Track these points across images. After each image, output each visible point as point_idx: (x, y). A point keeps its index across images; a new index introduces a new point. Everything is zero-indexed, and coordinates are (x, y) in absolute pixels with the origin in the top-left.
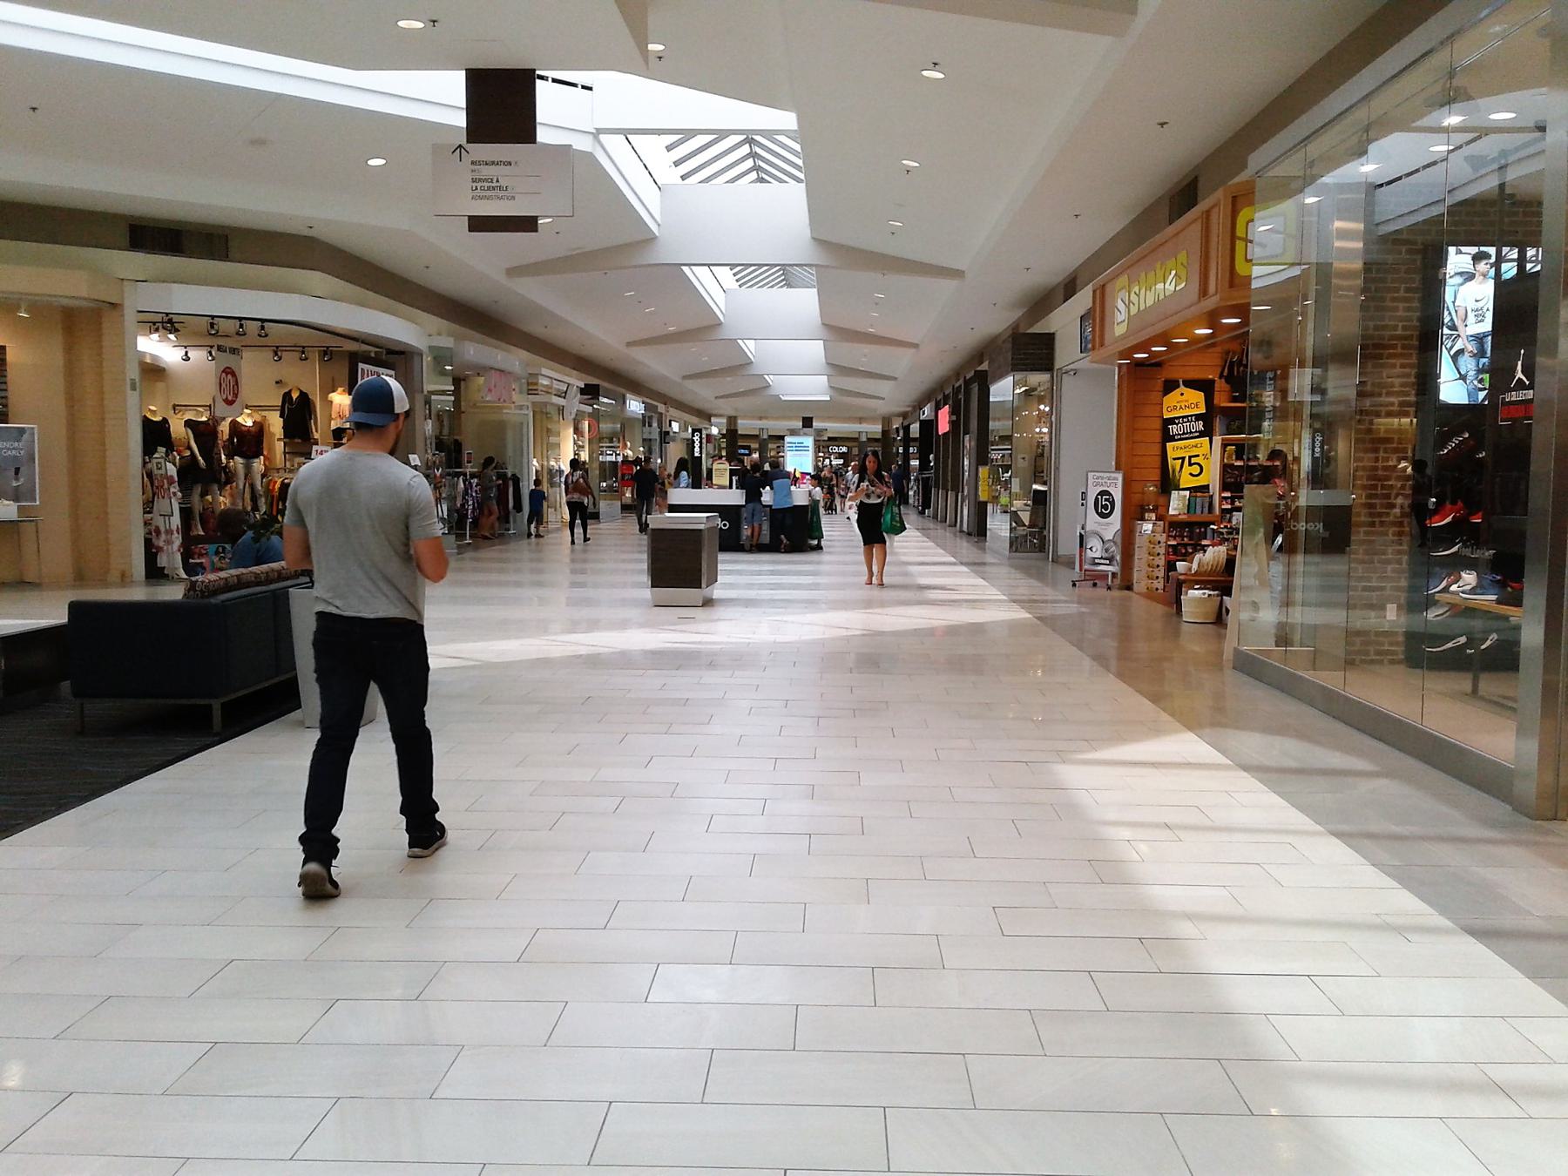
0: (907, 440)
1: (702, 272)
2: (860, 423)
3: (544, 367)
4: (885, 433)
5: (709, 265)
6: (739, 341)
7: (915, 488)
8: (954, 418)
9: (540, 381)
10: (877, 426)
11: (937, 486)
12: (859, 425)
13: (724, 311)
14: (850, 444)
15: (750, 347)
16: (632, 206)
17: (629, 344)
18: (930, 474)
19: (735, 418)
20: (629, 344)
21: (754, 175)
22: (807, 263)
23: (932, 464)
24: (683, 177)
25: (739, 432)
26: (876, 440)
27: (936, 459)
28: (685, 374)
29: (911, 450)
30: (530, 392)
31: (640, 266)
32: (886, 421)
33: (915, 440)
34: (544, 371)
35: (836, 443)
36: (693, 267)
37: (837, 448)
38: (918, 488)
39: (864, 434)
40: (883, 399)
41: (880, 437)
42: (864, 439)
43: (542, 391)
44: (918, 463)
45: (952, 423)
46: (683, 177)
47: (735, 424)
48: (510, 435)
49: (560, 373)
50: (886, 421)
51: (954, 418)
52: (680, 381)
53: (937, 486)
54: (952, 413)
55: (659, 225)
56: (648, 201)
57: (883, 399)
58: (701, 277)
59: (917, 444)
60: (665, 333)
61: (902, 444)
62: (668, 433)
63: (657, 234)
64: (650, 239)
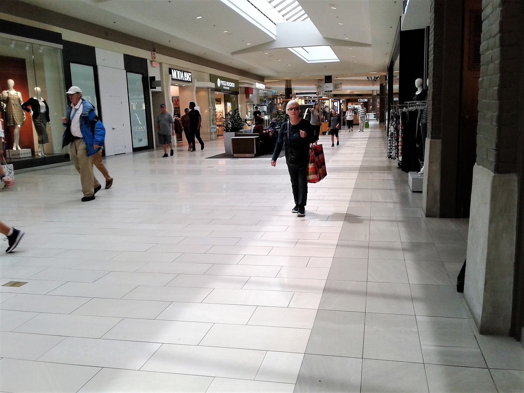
2: (373, 86)
12: (373, 87)
14: (369, 97)
19: (290, 81)
37: (362, 100)
38: (396, 129)
44: (398, 99)
47: (290, 85)
64: (273, 41)
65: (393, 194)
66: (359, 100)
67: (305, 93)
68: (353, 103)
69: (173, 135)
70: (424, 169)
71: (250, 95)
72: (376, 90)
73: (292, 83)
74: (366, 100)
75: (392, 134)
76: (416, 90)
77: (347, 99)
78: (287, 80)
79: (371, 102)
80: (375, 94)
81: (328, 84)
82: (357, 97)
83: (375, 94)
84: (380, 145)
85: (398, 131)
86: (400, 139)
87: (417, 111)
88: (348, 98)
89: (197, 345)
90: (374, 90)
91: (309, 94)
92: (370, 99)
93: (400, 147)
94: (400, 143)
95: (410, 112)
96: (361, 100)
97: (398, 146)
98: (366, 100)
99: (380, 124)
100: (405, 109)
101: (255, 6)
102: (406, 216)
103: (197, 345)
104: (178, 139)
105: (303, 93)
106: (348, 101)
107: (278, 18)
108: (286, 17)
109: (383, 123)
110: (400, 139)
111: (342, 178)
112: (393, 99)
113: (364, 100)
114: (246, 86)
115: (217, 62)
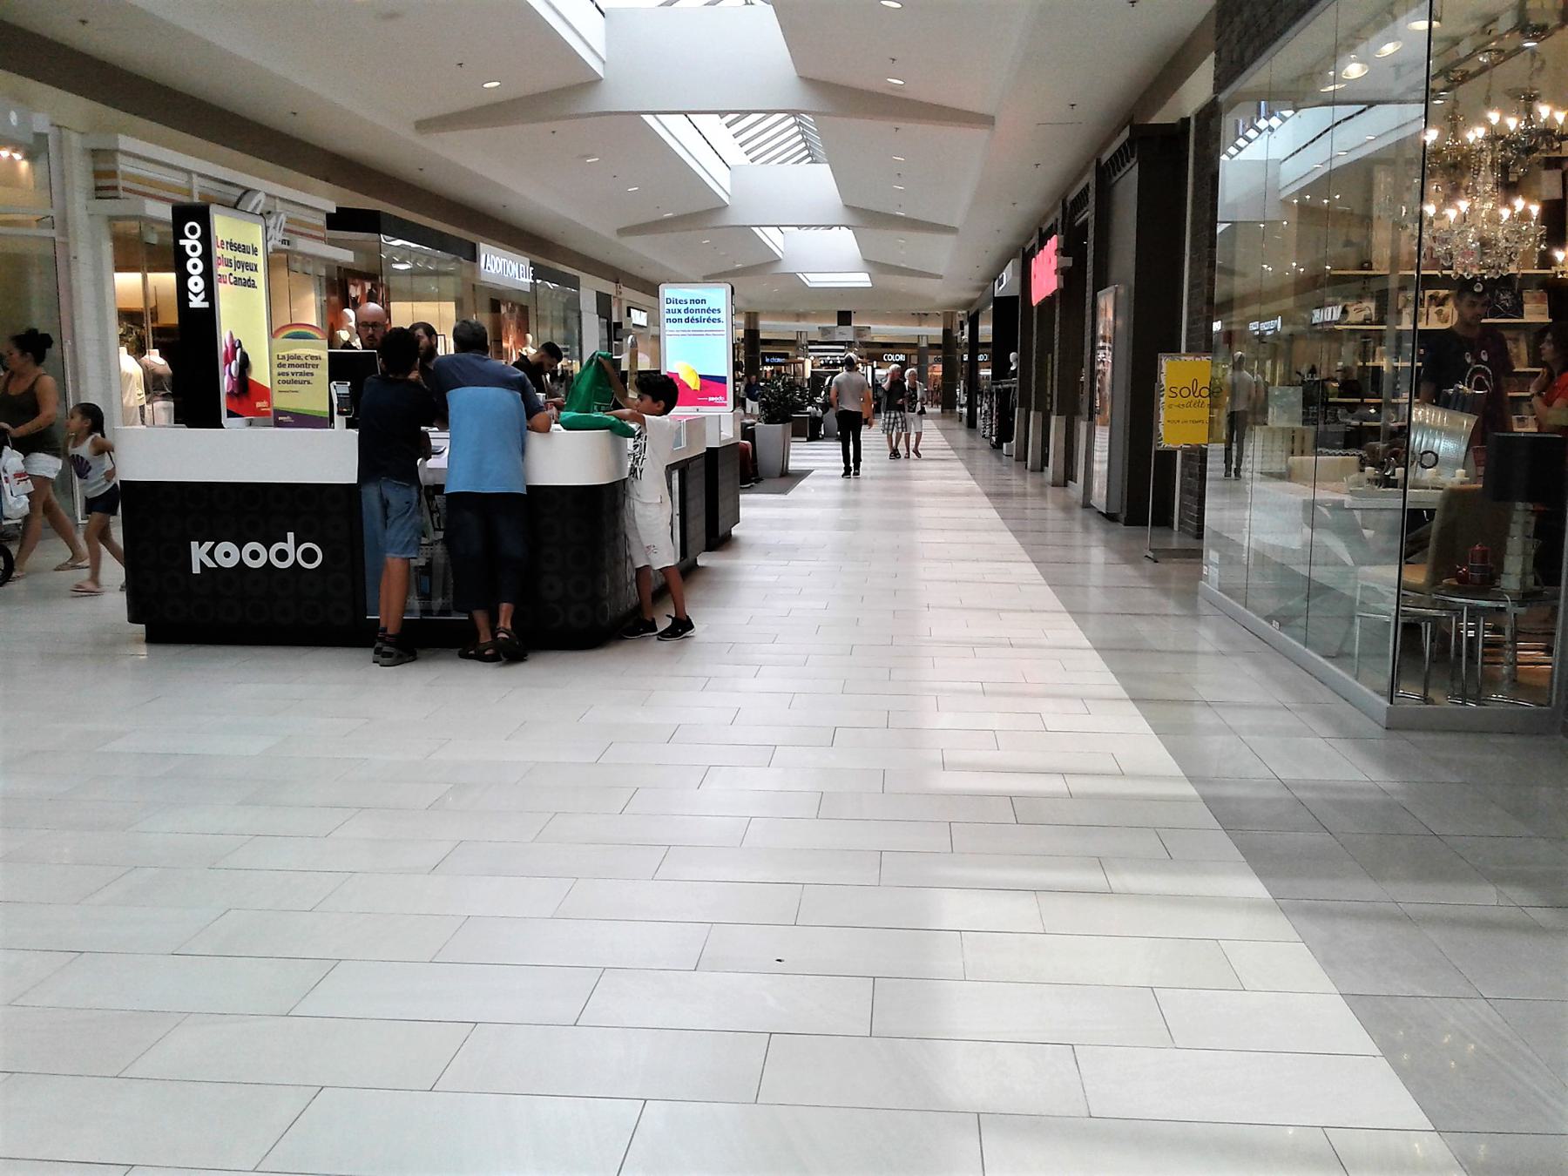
0: (974, 345)
1: (676, 123)
2: (920, 325)
3: (121, 132)
4: (947, 333)
5: (778, 226)
6: (755, 229)
7: (986, 406)
8: (1069, 262)
9: (121, 167)
10: (936, 329)
11: (1025, 403)
12: (918, 328)
13: (729, 192)
14: (909, 351)
15: (773, 238)
16: (583, 60)
17: (423, 126)
18: (1013, 383)
19: (756, 314)
20: (423, 126)
21: (809, 159)
22: (806, 109)
23: (1013, 368)
24: (752, 161)
25: (762, 336)
26: (938, 346)
27: (1024, 361)
28: (424, 115)
29: (981, 358)
30: (101, 194)
31: (719, 227)
32: (948, 317)
33: (986, 345)
34: (126, 143)
35: (891, 350)
36: (658, 116)
37: (892, 357)
38: (991, 407)
39: (924, 338)
40: (940, 277)
41: (941, 342)
42: (924, 344)
43: (125, 189)
44: (990, 373)
45: (1063, 272)
46: (752, 161)
47: (756, 323)
48: (36, 283)
49: (205, 158)
50: (948, 317)
51: (1069, 262)
52: (615, 238)
53: (1025, 403)
54: (1063, 251)
55: (604, 62)
56: (719, 179)
57: (940, 277)
58: (675, 131)
59: (990, 350)
60: (658, 218)
61: (967, 350)
62: (619, 325)
63: (602, 76)
64: (721, 208)
66: (886, 357)
70: (1014, 442)
72: (927, 336)
73: (760, 317)
75: (986, 412)
76: (1011, 365)
78: (749, 313)
83: (924, 344)
84: (885, 490)
85: (992, 409)
86: (994, 418)
87: (1010, 388)
89: (431, 1090)
93: (994, 426)
94: (994, 422)
95: (1004, 389)
97: (991, 425)
99: (942, 412)
100: (1000, 386)
102: (993, 489)
103: (431, 1090)
107: (735, 155)
108: (747, 147)
109: (948, 410)
110: (994, 418)
111: (232, 1081)
112: (977, 373)
113: (898, 358)
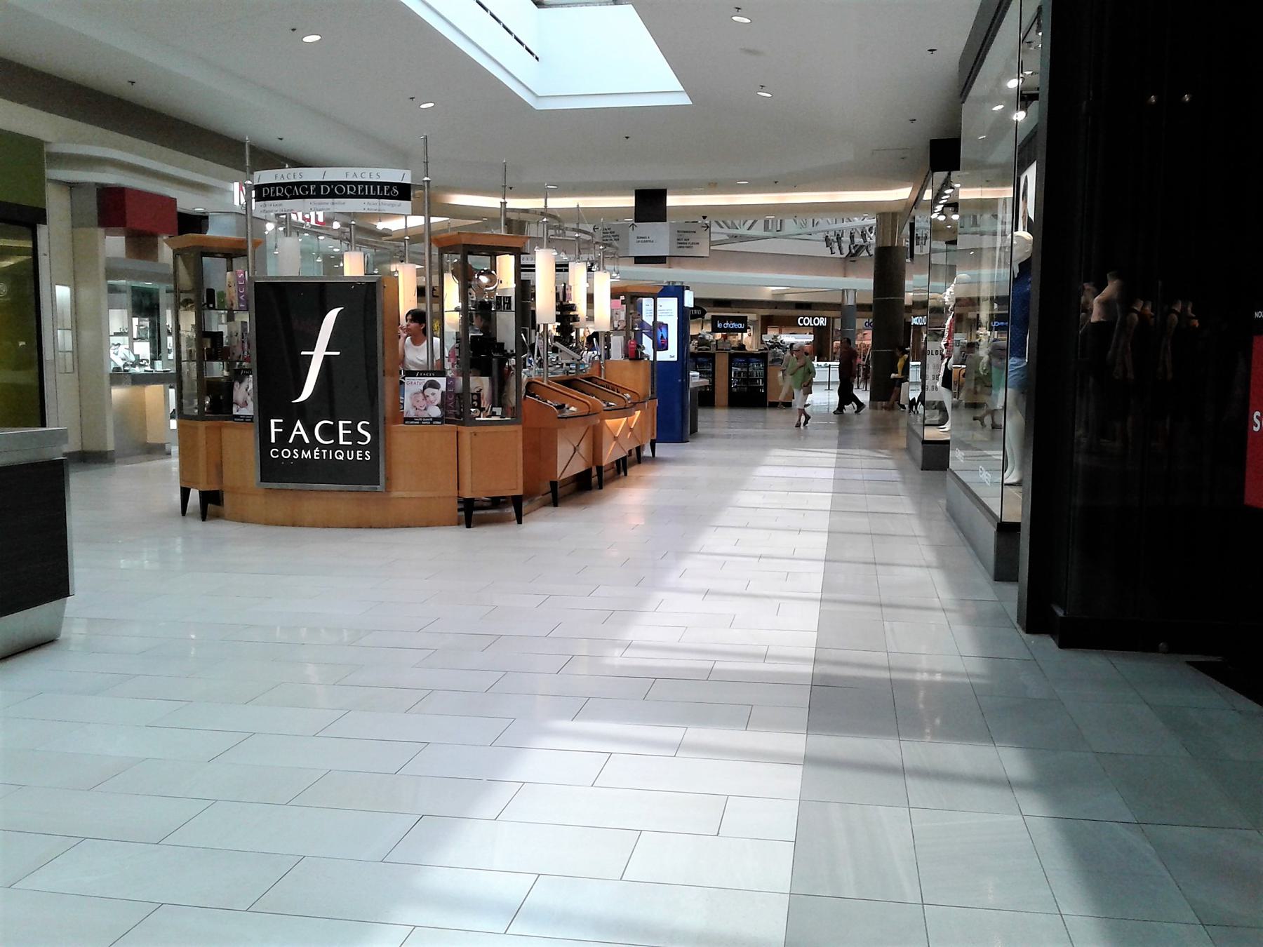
2: (845, 277)
14: (832, 314)
37: (810, 321)
65: (927, 740)
66: (802, 321)
67: (318, 184)
68: (783, 330)
69: (983, 363)
71: (347, 273)
72: (855, 290)
74: (822, 322)
77: (762, 317)
79: (836, 327)
80: (849, 304)
81: (646, 228)
82: (794, 312)
83: (850, 302)
88: (766, 312)
90: (847, 290)
91: (346, 196)
92: (833, 318)
96: (807, 321)
98: (822, 322)
101: (517, 36)
104: (346, 430)
105: (299, 184)
106: (767, 322)
113: (817, 321)
114: (110, 178)
115: (238, 139)
